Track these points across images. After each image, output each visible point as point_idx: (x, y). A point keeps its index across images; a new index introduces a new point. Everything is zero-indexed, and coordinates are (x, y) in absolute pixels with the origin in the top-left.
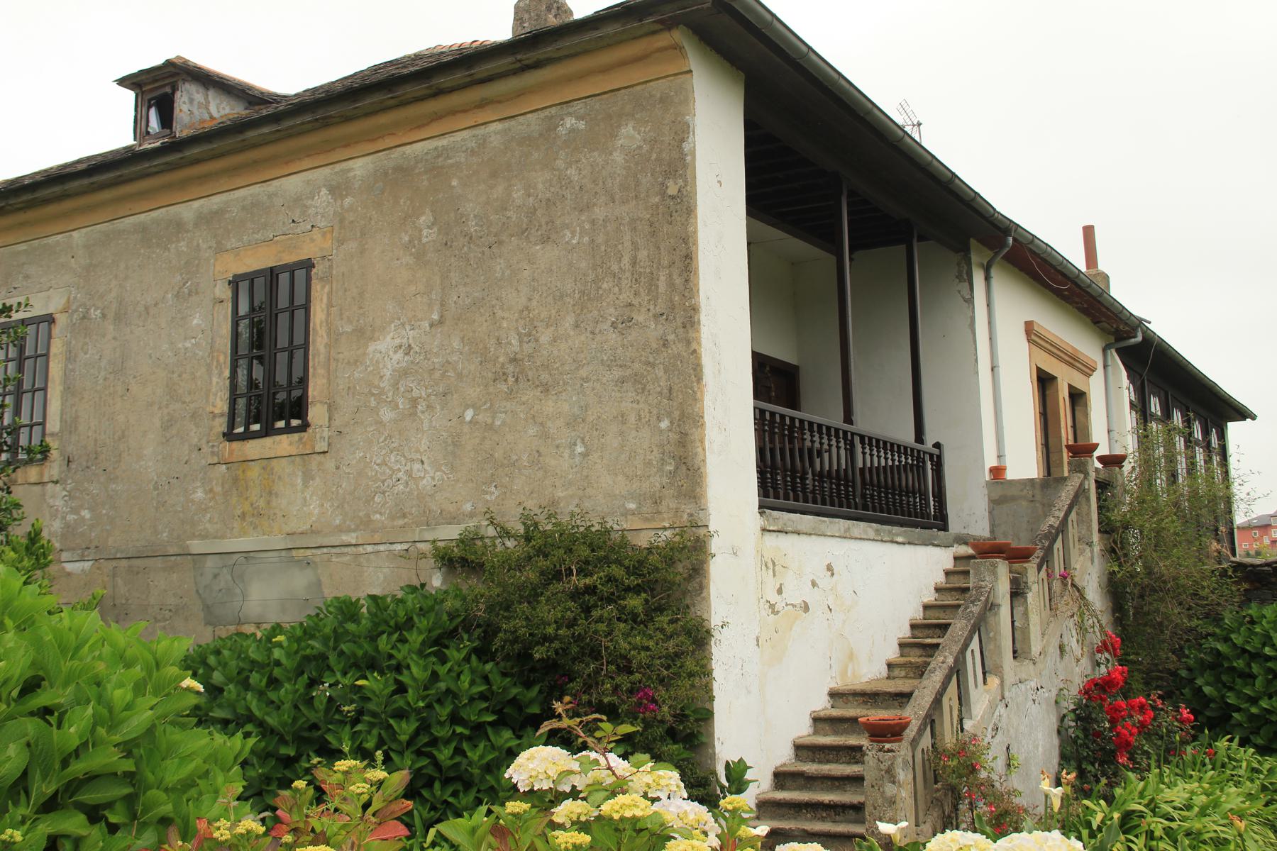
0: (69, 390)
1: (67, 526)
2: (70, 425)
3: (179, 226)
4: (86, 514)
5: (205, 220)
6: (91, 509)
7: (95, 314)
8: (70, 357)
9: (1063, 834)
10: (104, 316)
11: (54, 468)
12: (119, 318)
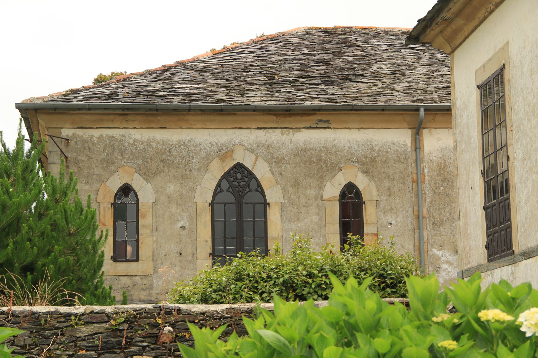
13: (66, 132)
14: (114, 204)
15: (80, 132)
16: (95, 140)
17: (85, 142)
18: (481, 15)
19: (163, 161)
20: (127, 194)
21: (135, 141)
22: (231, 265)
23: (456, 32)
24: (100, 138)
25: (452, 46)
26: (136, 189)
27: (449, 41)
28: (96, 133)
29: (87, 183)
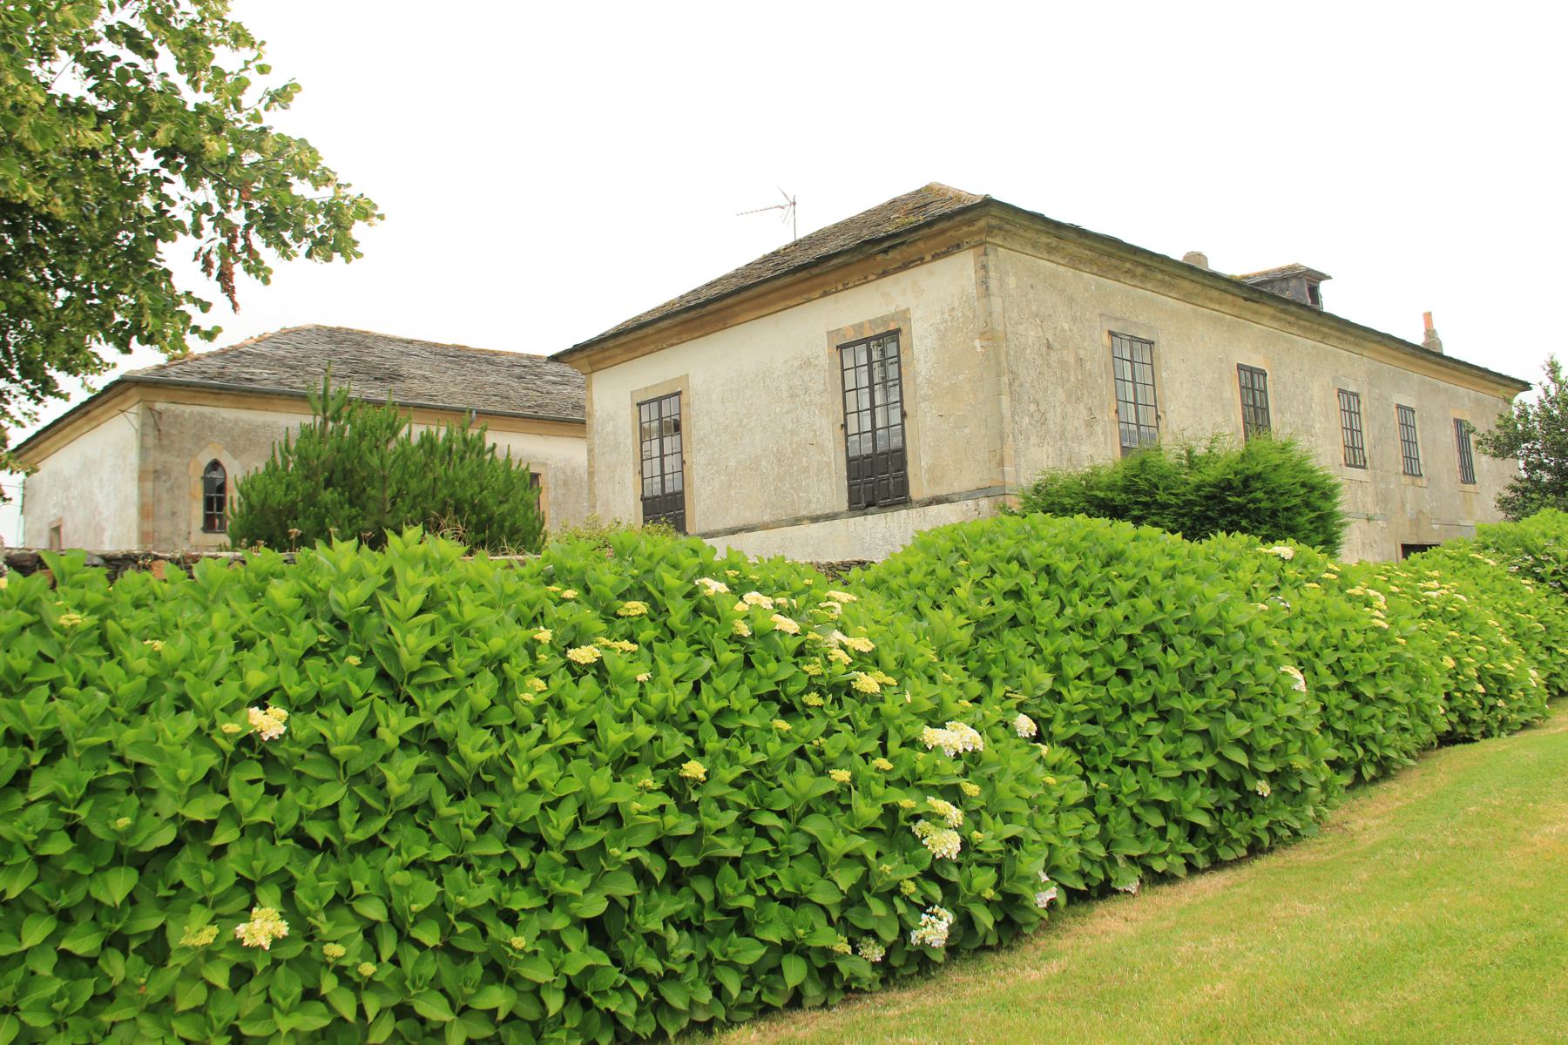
13: (159, 406)
14: (204, 478)
15: (172, 407)
16: (186, 415)
17: (177, 416)
18: (638, 353)
19: (250, 440)
20: (215, 469)
21: (224, 419)
22: (1050, 499)
23: (599, 362)
24: (191, 413)
25: (1253, 440)
26: (224, 465)
27: (591, 364)
28: (188, 409)
29: (178, 456)
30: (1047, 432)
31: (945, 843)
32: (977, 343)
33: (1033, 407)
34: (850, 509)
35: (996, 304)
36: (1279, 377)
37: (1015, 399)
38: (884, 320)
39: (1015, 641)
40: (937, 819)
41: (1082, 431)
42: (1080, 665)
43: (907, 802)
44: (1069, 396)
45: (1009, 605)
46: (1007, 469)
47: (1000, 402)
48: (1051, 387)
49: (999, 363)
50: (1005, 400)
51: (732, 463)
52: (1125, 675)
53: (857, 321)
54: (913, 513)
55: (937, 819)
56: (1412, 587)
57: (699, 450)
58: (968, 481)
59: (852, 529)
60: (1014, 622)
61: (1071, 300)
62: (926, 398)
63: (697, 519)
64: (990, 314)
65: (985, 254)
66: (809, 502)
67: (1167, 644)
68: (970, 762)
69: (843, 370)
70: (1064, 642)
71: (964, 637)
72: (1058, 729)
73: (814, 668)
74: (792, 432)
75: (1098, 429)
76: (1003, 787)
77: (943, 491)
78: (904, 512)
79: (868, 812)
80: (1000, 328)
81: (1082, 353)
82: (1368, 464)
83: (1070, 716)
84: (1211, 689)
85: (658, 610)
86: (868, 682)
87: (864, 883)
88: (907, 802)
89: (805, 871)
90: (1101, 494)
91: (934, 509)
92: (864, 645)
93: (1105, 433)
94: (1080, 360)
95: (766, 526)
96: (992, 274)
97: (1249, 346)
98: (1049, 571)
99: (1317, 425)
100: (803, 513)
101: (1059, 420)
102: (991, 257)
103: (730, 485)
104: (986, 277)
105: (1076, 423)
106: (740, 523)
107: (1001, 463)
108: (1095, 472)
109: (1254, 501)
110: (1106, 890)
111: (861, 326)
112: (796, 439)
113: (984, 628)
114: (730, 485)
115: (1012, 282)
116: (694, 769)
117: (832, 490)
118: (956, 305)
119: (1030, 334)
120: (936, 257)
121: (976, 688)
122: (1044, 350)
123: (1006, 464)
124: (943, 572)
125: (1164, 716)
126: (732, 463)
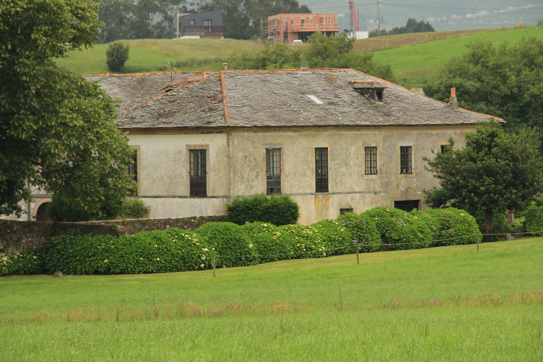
0: (415, 161)
1: (417, 185)
2: (416, 167)
3: (432, 134)
4: (420, 183)
5: (437, 134)
6: (421, 183)
7: (419, 147)
8: (415, 155)
9: (189, 145)
10: (421, 148)
11: (414, 175)
12: (423, 149)
30: (243, 180)
31: (204, 258)
32: (226, 158)
33: (240, 174)
34: (191, 196)
35: (231, 149)
36: (334, 148)
37: (235, 173)
38: (202, 146)
39: (214, 240)
40: (203, 256)
41: (254, 179)
42: (221, 243)
43: (200, 255)
44: (251, 169)
45: (214, 236)
46: (231, 192)
47: (230, 174)
48: (245, 168)
49: (230, 165)
50: (232, 174)
51: (154, 176)
52: (226, 244)
53: (194, 144)
54: (208, 199)
55: (203, 256)
56: (77, 261)
57: (143, 170)
58: (222, 193)
59: (191, 201)
60: (214, 237)
61: (254, 142)
62: (212, 170)
63: (142, 191)
64: (229, 152)
65: (229, 136)
66: (179, 192)
67: (232, 241)
68: (207, 252)
69: (190, 157)
70: (220, 240)
71: (208, 239)
72: (217, 250)
73: (192, 242)
74: (174, 171)
75: (260, 177)
76: (210, 254)
77: (215, 195)
78: (205, 199)
79: (197, 255)
80: (232, 155)
81: (256, 157)
82: (378, 172)
83: (219, 249)
84: (236, 247)
85: (179, 237)
86: (197, 244)
87: (197, 261)
88: (200, 255)
89: (192, 259)
90: (247, 205)
91: (213, 199)
92: (197, 240)
93: (262, 178)
94: (255, 159)
95: (165, 197)
96: (230, 141)
97: (321, 140)
98: (220, 231)
99: (351, 162)
100: (177, 195)
101: (247, 177)
102: (230, 137)
103: (153, 183)
104: (229, 142)
105: (253, 177)
106: (156, 195)
107: (230, 190)
108: (257, 195)
109: (274, 211)
110: (221, 267)
111: (195, 146)
112: (175, 173)
113: (210, 238)
114: (153, 183)
115: (236, 142)
116: (183, 251)
117: (185, 189)
118: (221, 147)
119: (240, 155)
120: (216, 133)
121: (208, 245)
122: (244, 158)
123: (231, 190)
124: (206, 231)
125: (231, 249)
126: (154, 176)
